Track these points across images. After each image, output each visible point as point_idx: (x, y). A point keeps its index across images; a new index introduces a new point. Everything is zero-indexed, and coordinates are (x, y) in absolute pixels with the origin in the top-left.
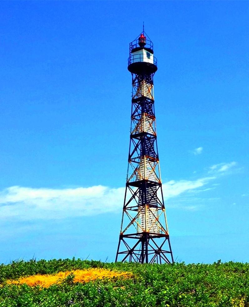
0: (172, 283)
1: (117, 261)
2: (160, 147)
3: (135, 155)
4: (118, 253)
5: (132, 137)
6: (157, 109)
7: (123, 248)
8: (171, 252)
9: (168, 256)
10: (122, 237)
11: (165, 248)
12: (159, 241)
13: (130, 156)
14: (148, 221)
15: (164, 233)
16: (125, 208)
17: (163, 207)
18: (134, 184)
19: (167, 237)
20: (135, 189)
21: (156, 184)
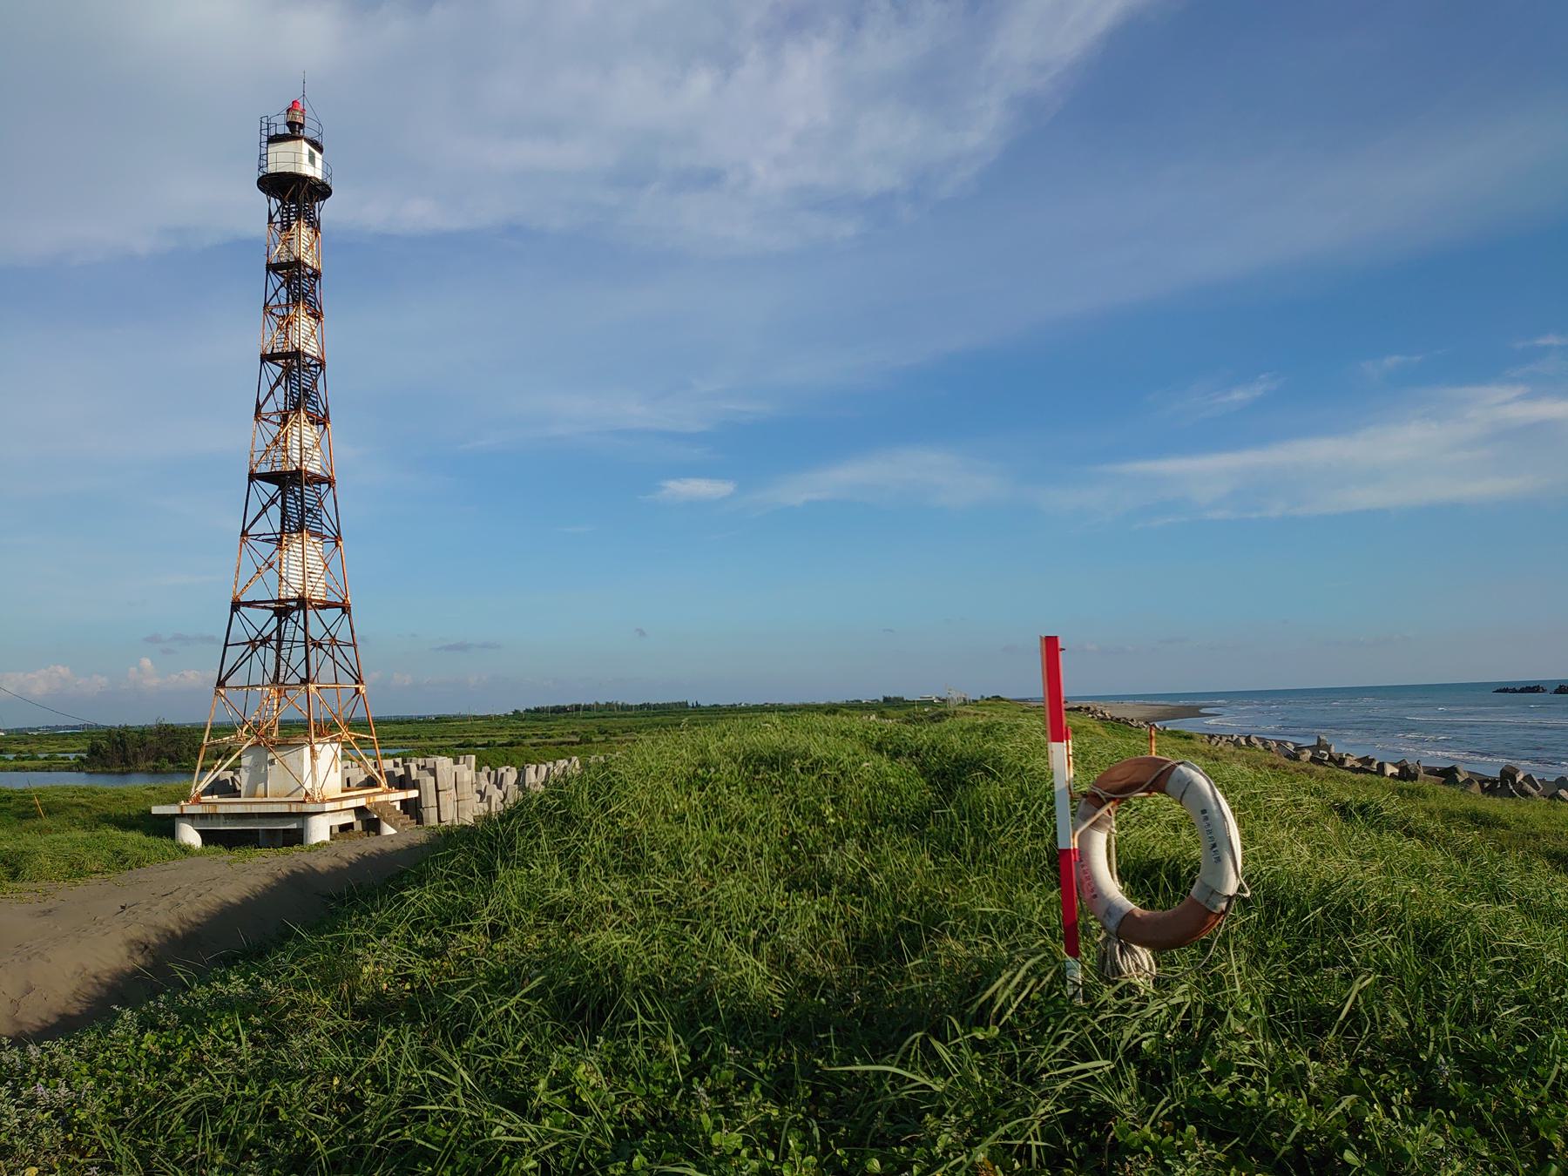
0: (592, 846)
1: (1065, 692)
2: (332, 389)
3: (262, 527)
4: (226, 645)
5: (265, 358)
6: (326, 293)
7: (238, 633)
8: (354, 645)
9: (349, 651)
10: (236, 606)
11: (343, 635)
12: (331, 615)
13: (259, 407)
14: (303, 567)
15: (333, 598)
16: (244, 533)
17: (337, 539)
18: (268, 477)
19: (345, 609)
20: (272, 489)
21: (318, 480)
